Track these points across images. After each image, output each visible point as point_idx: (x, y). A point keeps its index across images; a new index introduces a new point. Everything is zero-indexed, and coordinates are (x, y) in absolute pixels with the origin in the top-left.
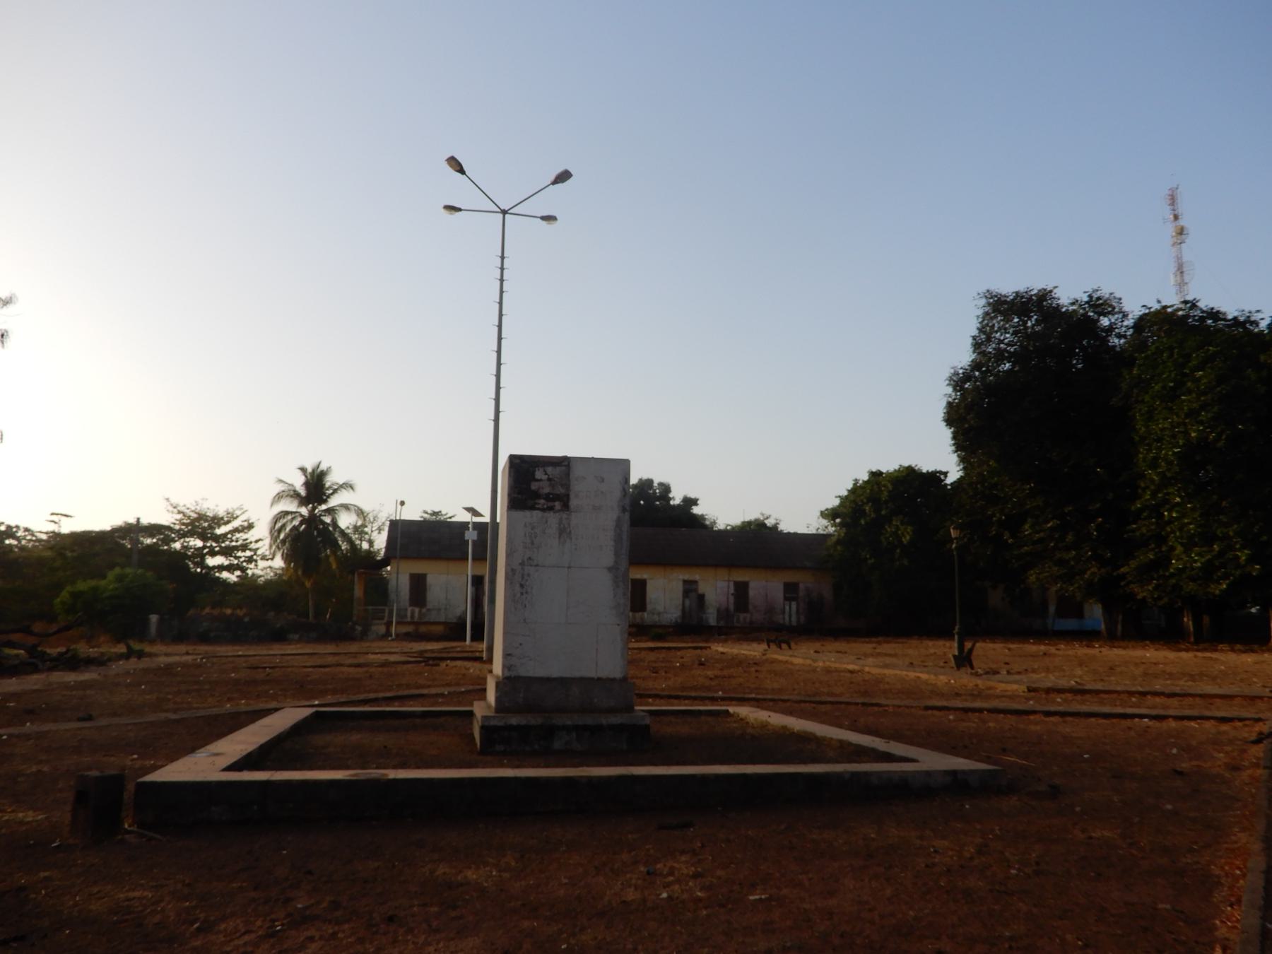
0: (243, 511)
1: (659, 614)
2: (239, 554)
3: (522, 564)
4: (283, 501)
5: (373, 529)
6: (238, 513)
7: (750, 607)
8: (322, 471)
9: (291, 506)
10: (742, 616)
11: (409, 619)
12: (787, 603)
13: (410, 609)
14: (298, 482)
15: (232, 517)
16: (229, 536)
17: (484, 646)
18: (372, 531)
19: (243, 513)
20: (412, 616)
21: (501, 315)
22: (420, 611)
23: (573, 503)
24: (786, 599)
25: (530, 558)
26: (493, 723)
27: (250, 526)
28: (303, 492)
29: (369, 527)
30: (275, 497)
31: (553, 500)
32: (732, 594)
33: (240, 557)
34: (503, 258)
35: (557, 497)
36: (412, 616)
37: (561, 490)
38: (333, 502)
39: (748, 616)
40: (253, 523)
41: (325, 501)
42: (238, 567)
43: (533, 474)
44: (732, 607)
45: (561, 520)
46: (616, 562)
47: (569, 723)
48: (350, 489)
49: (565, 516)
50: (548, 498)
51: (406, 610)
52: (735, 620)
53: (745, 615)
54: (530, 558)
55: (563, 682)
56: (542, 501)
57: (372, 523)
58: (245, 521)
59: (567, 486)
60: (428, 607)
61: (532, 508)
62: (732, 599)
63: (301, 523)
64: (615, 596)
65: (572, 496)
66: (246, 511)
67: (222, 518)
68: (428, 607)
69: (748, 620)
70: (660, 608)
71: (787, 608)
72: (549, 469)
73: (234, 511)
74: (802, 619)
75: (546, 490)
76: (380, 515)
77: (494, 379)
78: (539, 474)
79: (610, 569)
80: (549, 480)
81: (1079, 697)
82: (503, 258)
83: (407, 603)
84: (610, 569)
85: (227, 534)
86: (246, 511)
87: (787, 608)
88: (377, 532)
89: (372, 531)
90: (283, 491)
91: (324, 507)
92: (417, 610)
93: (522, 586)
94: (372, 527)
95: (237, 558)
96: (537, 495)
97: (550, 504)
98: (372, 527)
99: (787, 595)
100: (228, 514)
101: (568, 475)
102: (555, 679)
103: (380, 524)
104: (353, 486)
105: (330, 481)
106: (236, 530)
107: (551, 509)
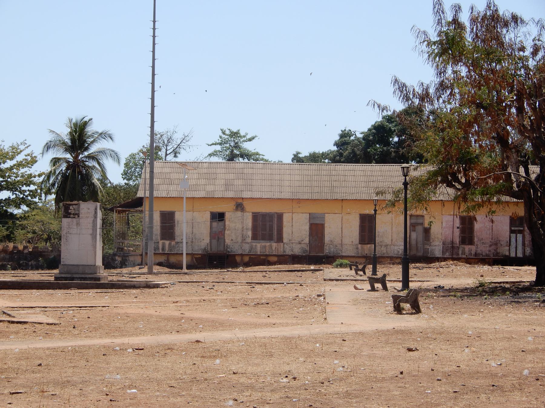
0: (26, 146)
1: (386, 246)
2: (24, 188)
3: (66, 233)
4: (51, 151)
5: (168, 152)
6: (22, 147)
7: (476, 239)
8: (86, 122)
9: (61, 154)
10: (467, 248)
11: (161, 252)
12: (513, 236)
13: (161, 242)
14: (64, 132)
15: (15, 151)
16: (15, 170)
17: (186, 271)
18: (166, 155)
19: (27, 147)
20: (163, 249)
21: (154, 59)
22: (170, 244)
23: (80, 216)
24: (512, 232)
25: (68, 232)
26: (57, 276)
27: (34, 161)
28: (69, 142)
29: (164, 150)
30: (45, 146)
31: (75, 215)
32: (458, 228)
33: (25, 191)
34: (154, 21)
35: (76, 214)
36: (163, 249)
37: (77, 212)
38: (93, 149)
39: (473, 248)
40: (35, 157)
41: (87, 149)
42: (23, 201)
43: (69, 208)
44: (457, 240)
45: (77, 221)
46: (93, 233)
47: (78, 276)
48: (109, 139)
49: (78, 219)
50: (73, 214)
51: (158, 242)
52: (460, 252)
53: (470, 246)
54: (68, 232)
55: (78, 265)
56: (72, 215)
57: (166, 146)
58: (28, 155)
59: (79, 211)
60: (176, 241)
61: (69, 217)
62: (457, 232)
63: (67, 169)
64: (93, 242)
65: (80, 214)
66: (30, 146)
67: (8, 153)
68: (176, 241)
69: (473, 253)
70: (387, 241)
71: (513, 240)
72: (74, 206)
73: (18, 145)
74: (528, 251)
75: (73, 212)
76: (175, 137)
77: (150, 101)
78: (71, 208)
79: (91, 234)
80: (74, 209)
81: (362, 282)
82: (154, 21)
83: (159, 238)
84: (91, 234)
85: (11, 168)
86: (30, 146)
87: (513, 240)
88: (173, 155)
89: (166, 155)
90: (50, 142)
91: (86, 153)
92: (167, 243)
93: (66, 240)
94: (167, 150)
95: (22, 192)
96: (70, 214)
97: (74, 216)
98: (167, 150)
99: (513, 228)
100: (13, 149)
101: (79, 207)
102: (75, 265)
103: (175, 146)
104: (113, 136)
105: (90, 129)
106: (20, 165)
107: (74, 217)
